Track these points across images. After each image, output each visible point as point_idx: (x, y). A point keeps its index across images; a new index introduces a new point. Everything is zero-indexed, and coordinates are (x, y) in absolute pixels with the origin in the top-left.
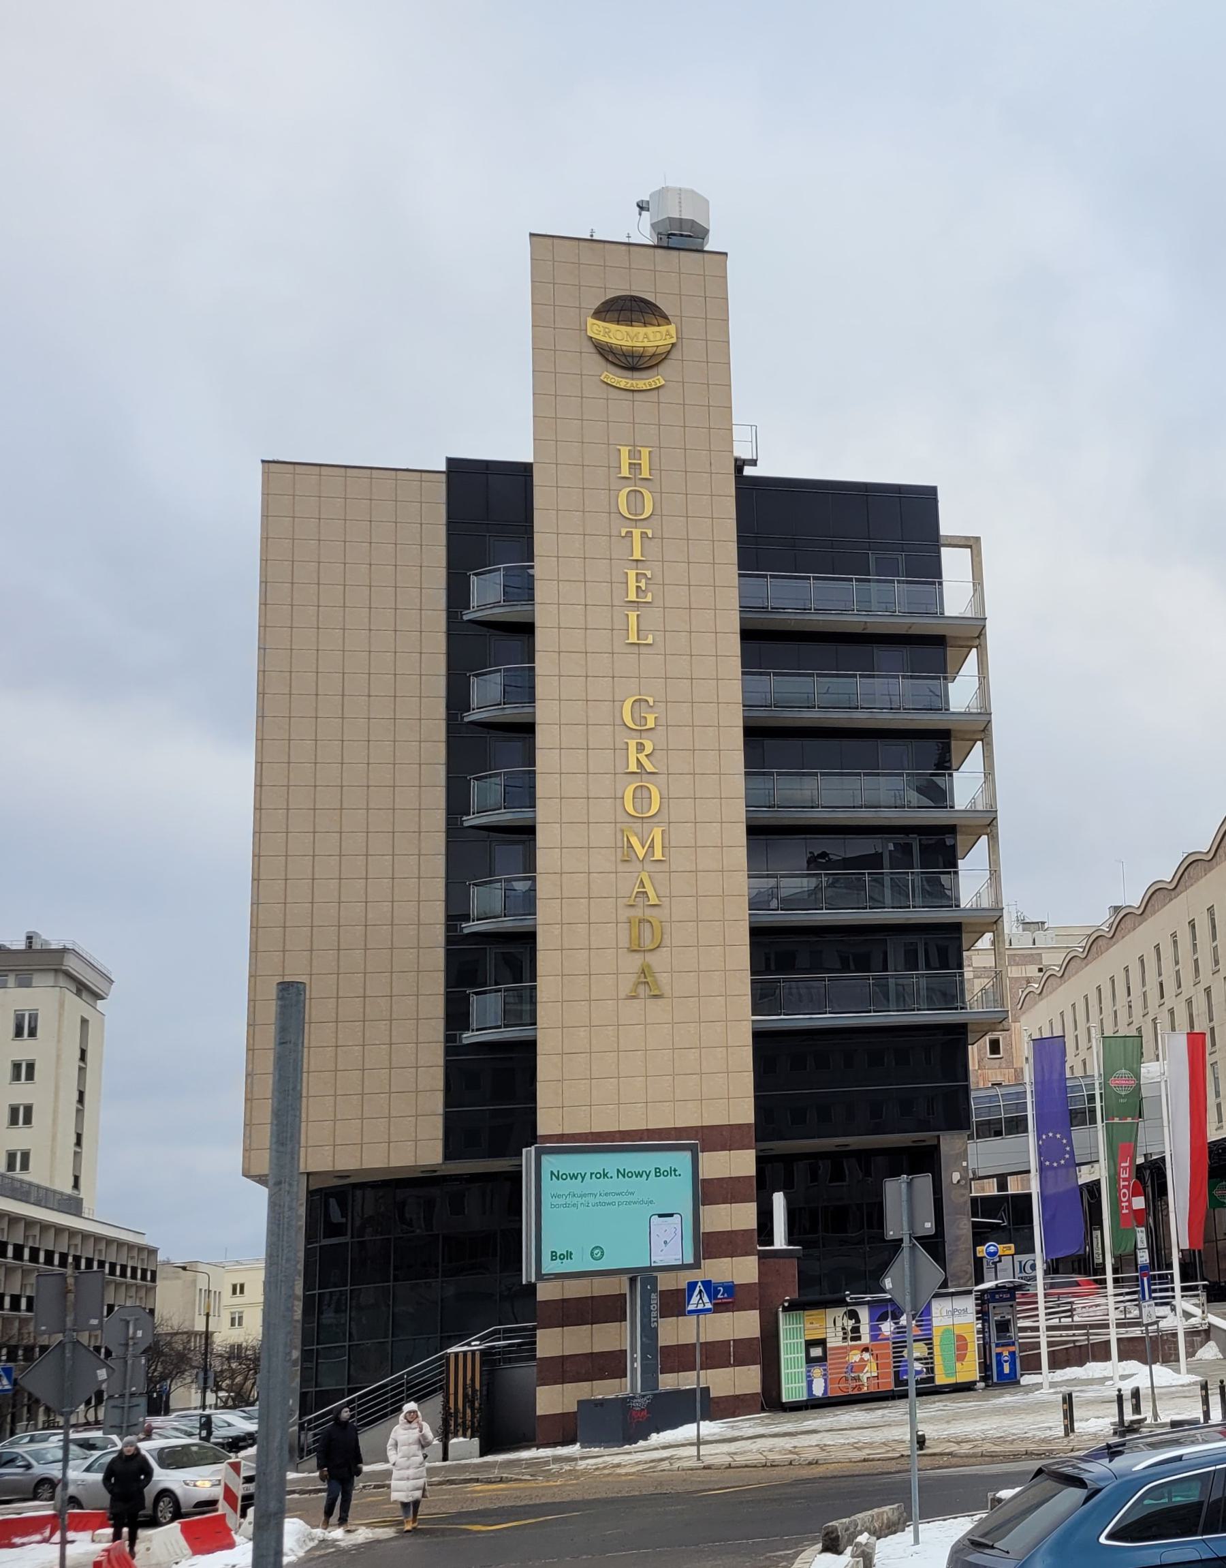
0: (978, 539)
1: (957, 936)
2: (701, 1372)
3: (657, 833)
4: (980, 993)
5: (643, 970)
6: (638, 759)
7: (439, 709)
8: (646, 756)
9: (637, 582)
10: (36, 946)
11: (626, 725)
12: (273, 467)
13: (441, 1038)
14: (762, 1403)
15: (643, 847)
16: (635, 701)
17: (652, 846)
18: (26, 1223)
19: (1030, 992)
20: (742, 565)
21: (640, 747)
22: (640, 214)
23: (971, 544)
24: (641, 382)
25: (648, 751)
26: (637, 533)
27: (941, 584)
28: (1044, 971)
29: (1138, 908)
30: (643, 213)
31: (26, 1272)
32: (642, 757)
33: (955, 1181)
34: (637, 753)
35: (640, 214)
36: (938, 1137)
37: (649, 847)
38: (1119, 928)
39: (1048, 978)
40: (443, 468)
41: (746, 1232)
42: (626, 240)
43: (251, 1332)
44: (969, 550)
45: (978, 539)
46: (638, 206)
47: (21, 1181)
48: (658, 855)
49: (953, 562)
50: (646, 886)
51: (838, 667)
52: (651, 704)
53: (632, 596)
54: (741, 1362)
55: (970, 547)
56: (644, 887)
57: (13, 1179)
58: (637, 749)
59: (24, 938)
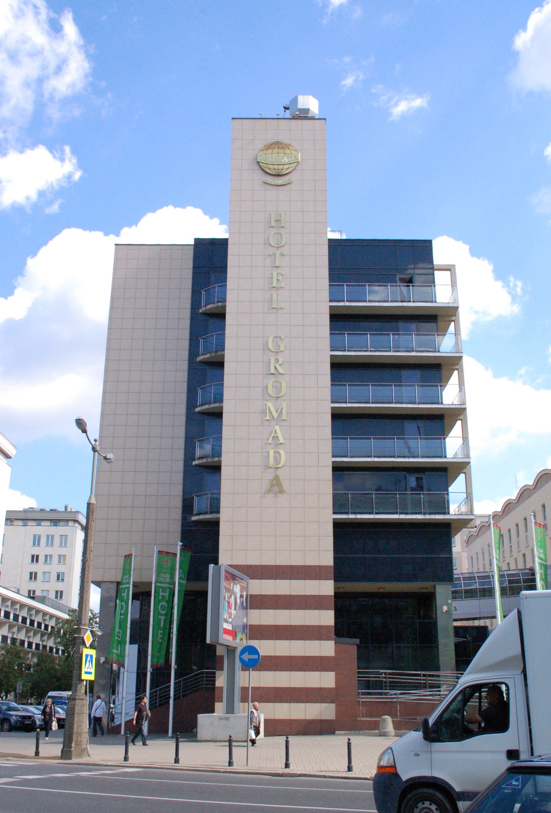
0: (454, 266)
1: (446, 474)
2: (248, 686)
3: (284, 405)
4: (457, 509)
5: (275, 478)
6: (275, 367)
7: (185, 355)
8: (280, 365)
9: (277, 277)
10: (69, 510)
11: (270, 349)
12: (119, 247)
13: (180, 518)
14: (35, 707)
15: (277, 413)
16: (274, 337)
17: (281, 413)
18: (50, 616)
19: (471, 535)
20: (331, 279)
21: (277, 361)
22: (285, 111)
23: (450, 269)
24: (280, 181)
25: (280, 363)
26: (278, 253)
27: (434, 286)
28: (477, 527)
29: (532, 485)
30: (287, 111)
31: (19, 630)
32: (277, 366)
33: (444, 611)
34: (275, 364)
35: (285, 111)
36: (435, 587)
37: (280, 413)
38: (521, 498)
39: (481, 527)
40: (193, 243)
41: (328, 627)
42: (277, 117)
43: (116, 669)
44: (449, 272)
45: (454, 266)
46: (284, 108)
47: (59, 603)
48: (284, 417)
49: (441, 277)
50: (278, 433)
51: (379, 382)
52: (283, 338)
53: (275, 284)
54: (323, 701)
55: (449, 270)
56: (277, 434)
57: (56, 602)
58: (275, 362)
59: (64, 507)
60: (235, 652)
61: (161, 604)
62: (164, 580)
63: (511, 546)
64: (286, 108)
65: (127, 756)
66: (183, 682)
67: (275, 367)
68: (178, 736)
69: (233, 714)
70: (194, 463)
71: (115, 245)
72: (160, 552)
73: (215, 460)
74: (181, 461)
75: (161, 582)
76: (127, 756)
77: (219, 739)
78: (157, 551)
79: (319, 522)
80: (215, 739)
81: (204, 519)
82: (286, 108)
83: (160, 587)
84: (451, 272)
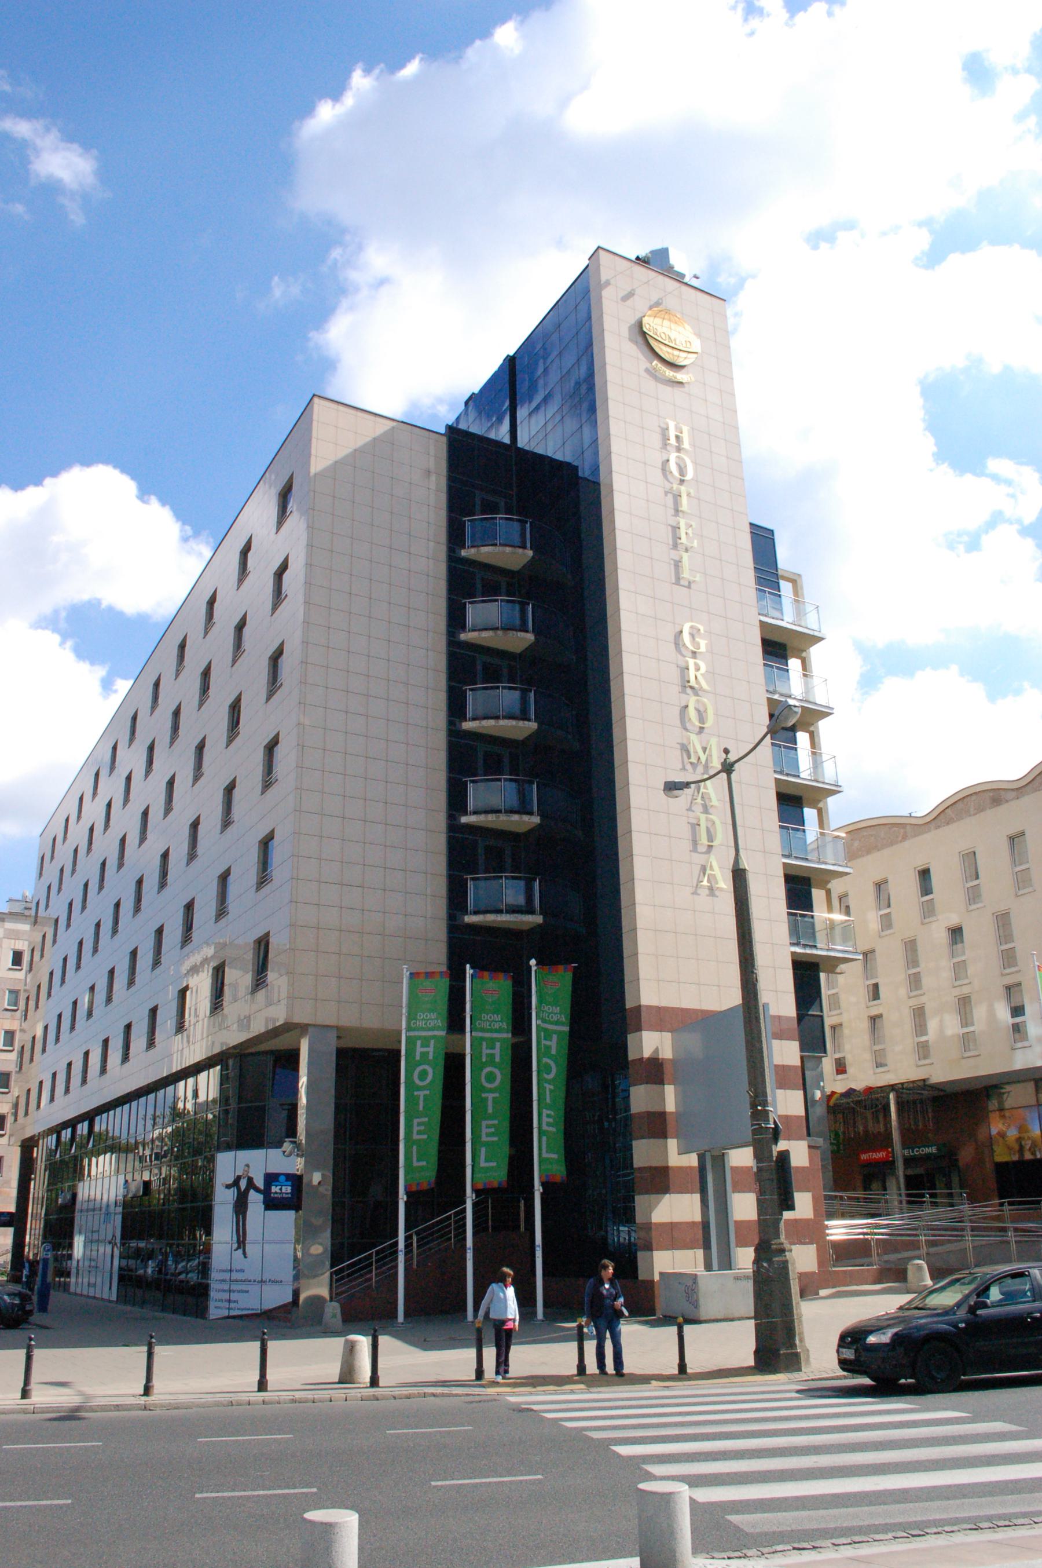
60: (724, 1161)
61: (485, 1071)
62: (490, 1025)
63: (876, 986)
64: (696, 277)
65: (28, 1388)
66: (455, 1217)
67: (696, 677)
68: (266, 1337)
69: (731, 1269)
70: (464, 820)
71: (751, 524)
72: (413, 975)
73: (513, 819)
74: (442, 814)
75: (483, 1030)
76: (28, 1388)
77: (737, 1315)
78: (408, 973)
79: (675, 933)
80: (731, 1316)
81: (494, 921)
82: (696, 277)
83: (483, 1039)
84: (441, 434)
